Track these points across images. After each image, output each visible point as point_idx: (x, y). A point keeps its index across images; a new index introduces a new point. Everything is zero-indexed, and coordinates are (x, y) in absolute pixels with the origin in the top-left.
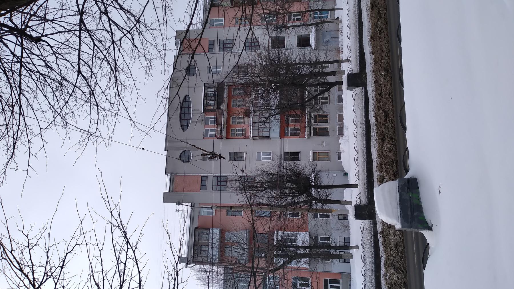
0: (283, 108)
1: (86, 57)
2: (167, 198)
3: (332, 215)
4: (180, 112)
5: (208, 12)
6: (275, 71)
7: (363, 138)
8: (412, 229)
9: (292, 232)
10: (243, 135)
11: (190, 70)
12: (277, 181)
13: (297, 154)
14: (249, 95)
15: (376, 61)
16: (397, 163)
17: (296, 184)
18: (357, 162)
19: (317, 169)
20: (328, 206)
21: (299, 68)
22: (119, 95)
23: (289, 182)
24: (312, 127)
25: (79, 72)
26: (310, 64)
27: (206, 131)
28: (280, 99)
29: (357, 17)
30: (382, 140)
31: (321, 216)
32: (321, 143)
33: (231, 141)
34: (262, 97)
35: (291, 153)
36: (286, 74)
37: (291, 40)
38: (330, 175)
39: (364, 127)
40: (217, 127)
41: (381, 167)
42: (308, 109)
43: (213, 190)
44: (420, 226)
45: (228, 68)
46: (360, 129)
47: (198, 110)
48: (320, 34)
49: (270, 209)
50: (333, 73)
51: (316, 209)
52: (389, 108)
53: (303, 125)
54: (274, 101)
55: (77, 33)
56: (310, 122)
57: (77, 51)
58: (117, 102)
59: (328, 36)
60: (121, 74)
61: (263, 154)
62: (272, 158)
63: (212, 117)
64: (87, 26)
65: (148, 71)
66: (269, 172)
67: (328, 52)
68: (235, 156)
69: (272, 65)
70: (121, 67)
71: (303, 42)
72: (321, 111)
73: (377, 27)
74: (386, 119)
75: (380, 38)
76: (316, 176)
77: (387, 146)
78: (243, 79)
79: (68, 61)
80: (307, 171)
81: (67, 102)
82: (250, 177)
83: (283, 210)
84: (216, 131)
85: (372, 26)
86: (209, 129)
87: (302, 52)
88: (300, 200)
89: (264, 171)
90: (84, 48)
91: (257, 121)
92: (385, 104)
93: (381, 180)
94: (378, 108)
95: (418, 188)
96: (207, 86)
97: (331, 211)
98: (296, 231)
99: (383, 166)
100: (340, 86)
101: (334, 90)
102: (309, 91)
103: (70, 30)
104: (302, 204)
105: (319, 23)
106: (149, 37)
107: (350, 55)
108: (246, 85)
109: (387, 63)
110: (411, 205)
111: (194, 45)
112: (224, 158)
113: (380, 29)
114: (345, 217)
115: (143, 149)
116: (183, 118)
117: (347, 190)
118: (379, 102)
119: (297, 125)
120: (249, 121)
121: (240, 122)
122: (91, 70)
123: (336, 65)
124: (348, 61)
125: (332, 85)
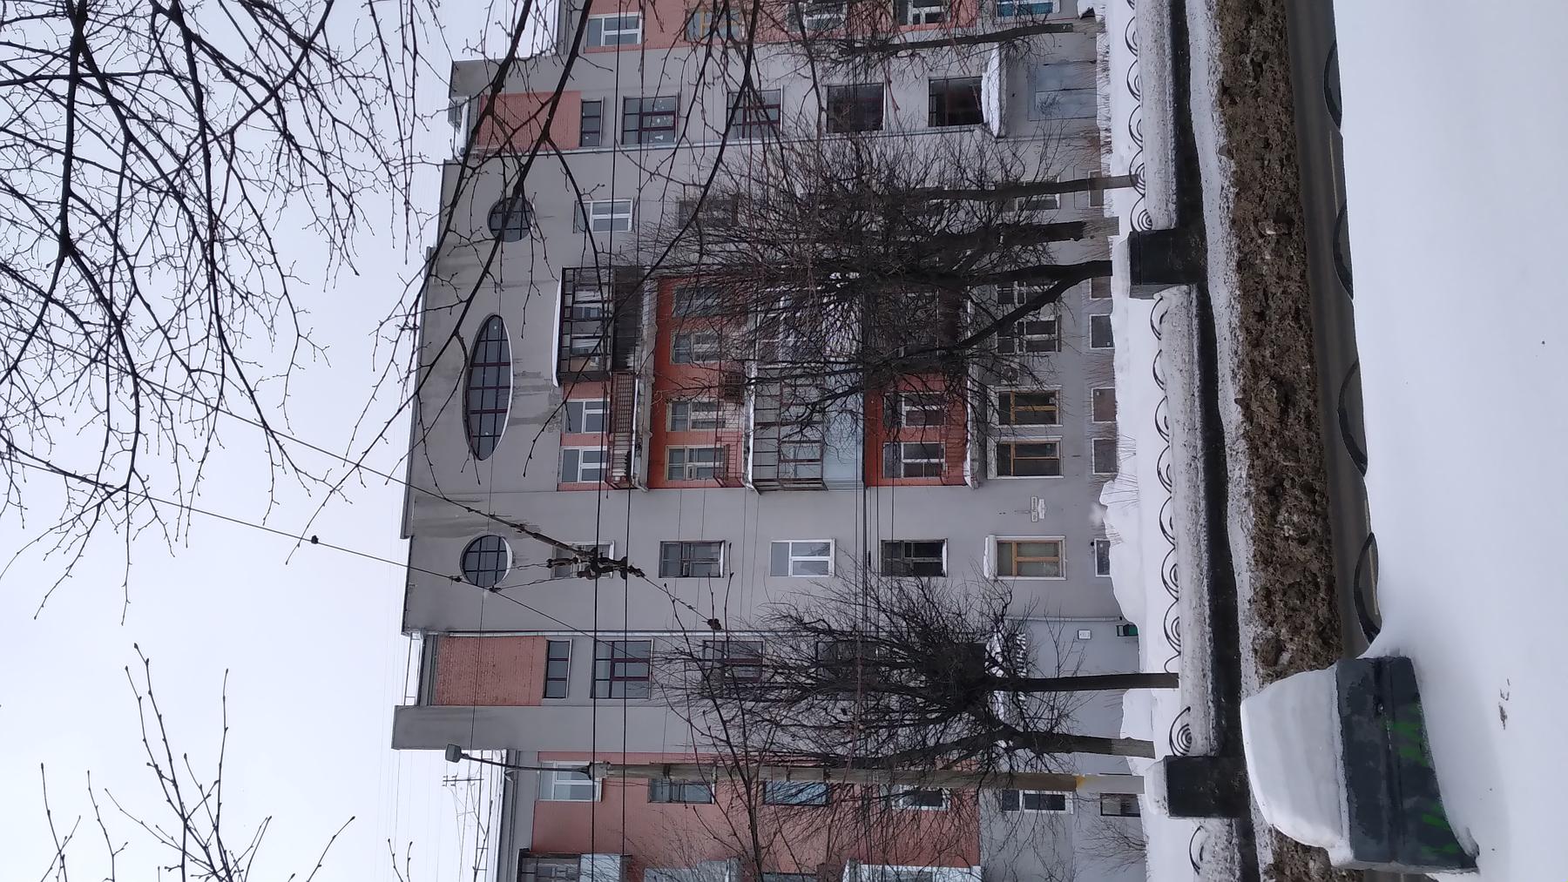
0: (877, 369)
1: (89, 182)
2: (411, 730)
3: (1076, 799)
4: (464, 382)
5: (577, 16)
6: (843, 223)
7: (1196, 487)
8: (1394, 866)
9: (915, 868)
10: (715, 474)
11: (512, 216)
12: (851, 662)
13: (934, 548)
14: (739, 314)
15: (1241, 183)
16: (1330, 588)
17: (931, 673)
18: (1171, 582)
19: (1016, 609)
20: (1058, 763)
21: (939, 209)
22: (221, 336)
23: (900, 667)
24: (992, 444)
25: (68, 247)
26: (981, 194)
27: (570, 459)
28: (865, 332)
29: (1166, 12)
30: (1271, 493)
31: (1032, 802)
32: (1028, 507)
33: (667, 498)
34: (792, 325)
35: (908, 545)
36: (889, 231)
37: (908, 99)
38: (1068, 631)
39: (1199, 443)
40: (612, 444)
41: (1270, 605)
42: (974, 371)
43: (593, 696)
44: (1425, 850)
45: (660, 211)
46: (1183, 453)
47: (537, 375)
48: (1022, 74)
49: (827, 776)
50: (1073, 231)
51: (1011, 775)
52: (1298, 367)
53: (955, 434)
54: (842, 342)
55: (61, 87)
56: (981, 421)
57: (60, 159)
58: (213, 365)
59: (1052, 84)
60: (234, 250)
61: (798, 549)
62: (831, 567)
63: (590, 403)
64: (100, 60)
65: (339, 239)
66: (820, 626)
67: (1053, 144)
68: (686, 559)
69: (830, 199)
70: (234, 223)
71: (955, 106)
72: (1028, 380)
73: (1244, 49)
74: (1284, 412)
75: (1257, 94)
76: (1010, 641)
77: (1290, 521)
78: (721, 253)
79: (21, 197)
80: (974, 620)
81: (15, 367)
82: (744, 644)
83: (878, 778)
84: (608, 457)
85: (1225, 45)
86: (582, 449)
87: (948, 145)
88: (949, 739)
89: (800, 621)
90: (86, 145)
91: (771, 417)
92: (1282, 353)
93: (1271, 657)
94: (1253, 370)
95: (1416, 697)
96: (572, 281)
97: (1070, 783)
98: (931, 863)
99: (1276, 598)
100: (1102, 279)
101: (1078, 296)
102: (980, 300)
103: (34, 78)
104: (955, 755)
105: (1015, 33)
106: (346, 108)
107: (1139, 161)
108: (731, 276)
109: (1287, 189)
110: (1389, 766)
111: (523, 141)
112: (639, 573)
113: (1258, 58)
114: (1128, 807)
115: (315, 540)
116: (475, 406)
117: (1133, 698)
118: (1256, 343)
119: (933, 435)
120: (742, 419)
121: (706, 423)
122: (114, 236)
123: (1083, 197)
124: (1132, 181)
125: (1069, 276)
